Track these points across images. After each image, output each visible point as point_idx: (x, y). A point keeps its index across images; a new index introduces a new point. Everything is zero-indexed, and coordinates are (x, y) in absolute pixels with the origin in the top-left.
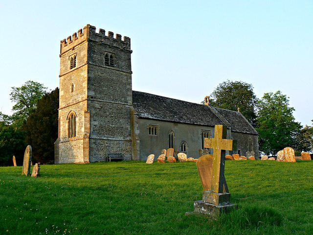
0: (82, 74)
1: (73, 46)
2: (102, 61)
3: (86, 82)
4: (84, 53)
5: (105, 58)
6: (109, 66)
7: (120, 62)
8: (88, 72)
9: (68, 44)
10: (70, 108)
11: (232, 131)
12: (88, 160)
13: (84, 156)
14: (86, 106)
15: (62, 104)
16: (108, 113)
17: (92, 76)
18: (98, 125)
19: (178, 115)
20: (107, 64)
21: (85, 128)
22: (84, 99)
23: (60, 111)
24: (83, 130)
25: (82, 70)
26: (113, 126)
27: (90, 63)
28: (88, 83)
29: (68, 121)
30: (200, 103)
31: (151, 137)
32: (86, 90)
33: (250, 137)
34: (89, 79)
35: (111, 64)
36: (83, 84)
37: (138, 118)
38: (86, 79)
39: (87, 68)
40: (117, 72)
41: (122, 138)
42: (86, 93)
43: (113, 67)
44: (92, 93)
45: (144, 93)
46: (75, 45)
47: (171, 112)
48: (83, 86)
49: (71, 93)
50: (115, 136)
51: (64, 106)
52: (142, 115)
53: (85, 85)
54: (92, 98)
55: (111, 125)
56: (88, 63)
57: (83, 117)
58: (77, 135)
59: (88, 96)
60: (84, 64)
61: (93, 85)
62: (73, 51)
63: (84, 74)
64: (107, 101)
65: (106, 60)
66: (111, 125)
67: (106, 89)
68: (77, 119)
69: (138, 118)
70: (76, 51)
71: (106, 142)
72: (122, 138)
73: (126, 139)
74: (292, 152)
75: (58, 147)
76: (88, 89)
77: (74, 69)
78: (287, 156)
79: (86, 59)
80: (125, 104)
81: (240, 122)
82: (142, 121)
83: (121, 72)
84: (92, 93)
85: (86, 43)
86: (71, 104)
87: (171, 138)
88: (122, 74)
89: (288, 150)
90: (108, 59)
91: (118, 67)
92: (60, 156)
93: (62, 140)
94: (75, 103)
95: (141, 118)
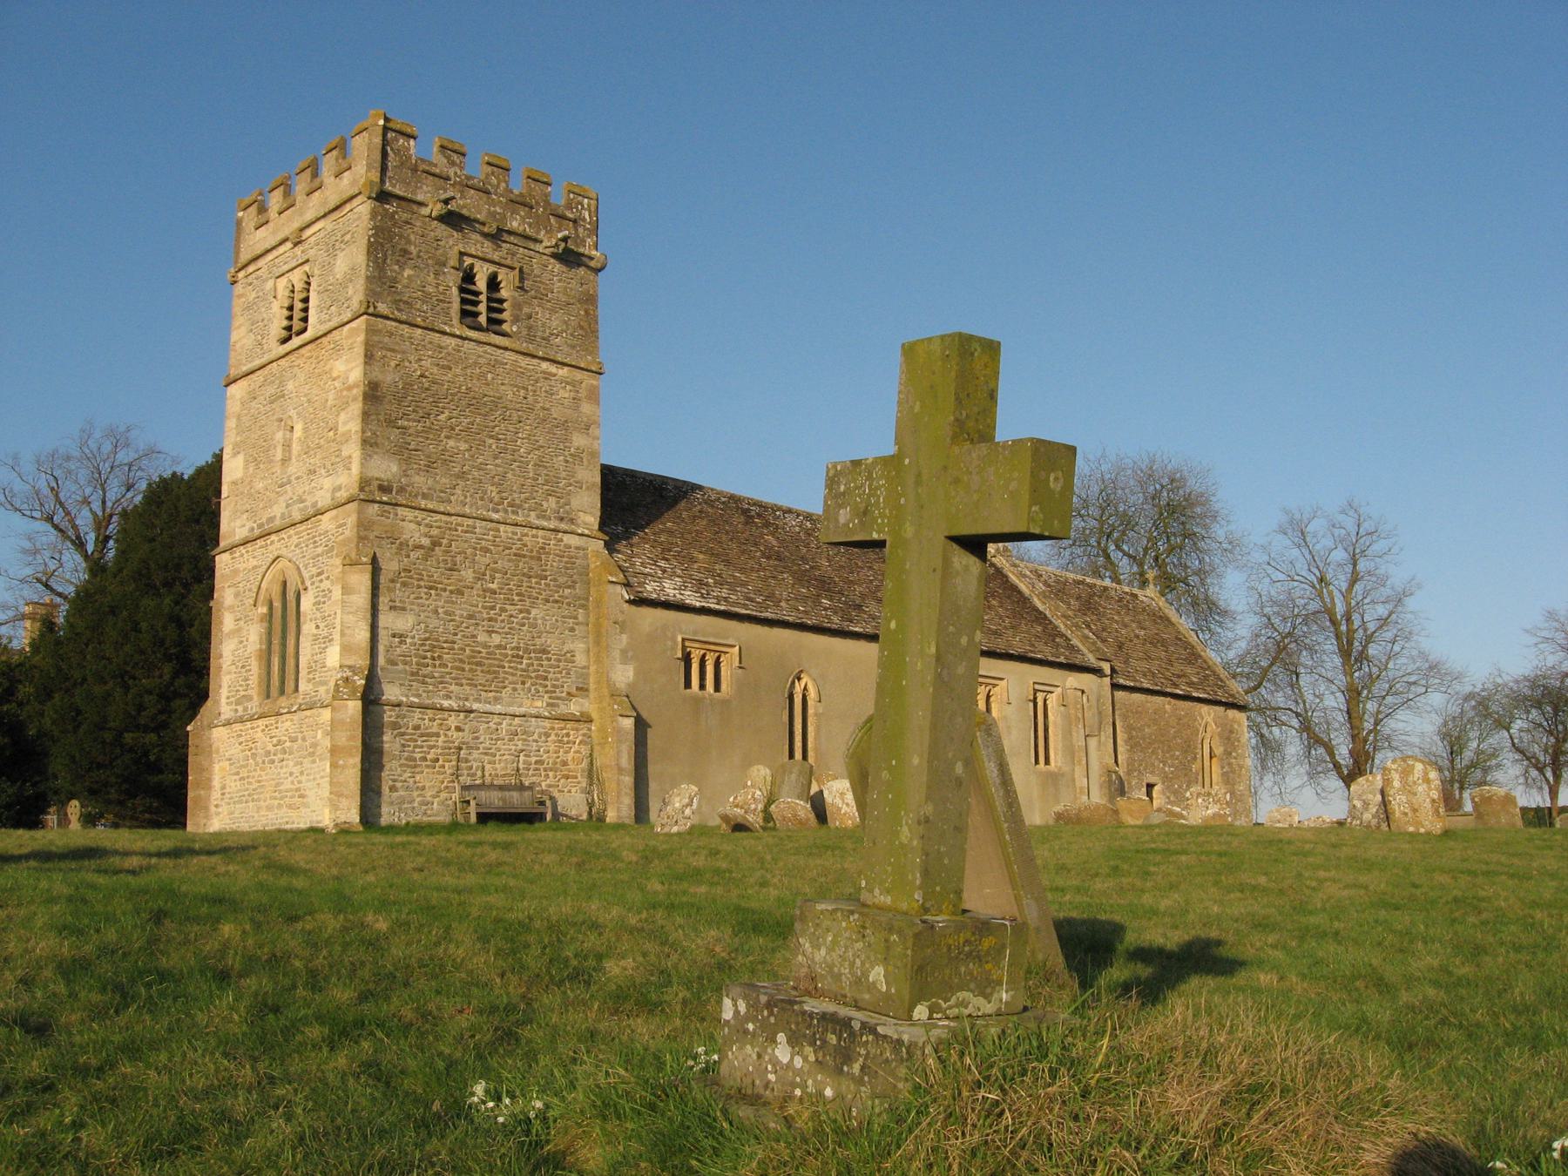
0: (339, 366)
1: (297, 225)
2: (444, 301)
3: (356, 408)
4: (351, 261)
5: (462, 290)
6: (478, 328)
7: (541, 315)
8: (369, 357)
9: (273, 213)
10: (275, 545)
11: (1115, 686)
12: (354, 816)
13: (337, 793)
14: (349, 531)
15: (233, 523)
16: (468, 575)
17: (388, 378)
18: (419, 635)
19: (841, 593)
20: (468, 315)
21: (346, 649)
22: (343, 495)
23: (223, 562)
24: (333, 656)
25: (338, 349)
26: (496, 639)
27: (382, 308)
28: (366, 415)
29: (263, 610)
30: (807, 497)
31: (697, 701)
32: (353, 450)
33: (1208, 714)
34: (373, 394)
35: (490, 320)
36: (343, 417)
37: (630, 602)
38: (358, 392)
39: (361, 338)
40: (524, 362)
41: (540, 705)
42: (355, 468)
43: (504, 334)
44: (386, 468)
45: (665, 480)
46: (309, 216)
47: (801, 577)
48: (341, 429)
49: (277, 469)
50: (505, 694)
51: (241, 533)
52: (650, 589)
53: (350, 422)
54: (386, 489)
55: (482, 637)
56: (369, 311)
57: (337, 593)
58: (302, 687)
59: (364, 483)
60: (349, 315)
61: (391, 423)
62: (298, 250)
63: (349, 368)
64: (467, 510)
65: (463, 301)
66: (482, 637)
67: (463, 446)
68: (307, 603)
69: (630, 602)
70: (310, 249)
71: (453, 721)
72: (540, 705)
73: (563, 709)
74: (1427, 781)
75: (208, 751)
76: (365, 442)
77: (296, 341)
78: (1398, 803)
79: (356, 294)
80: (563, 526)
81: (1157, 641)
82: (650, 618)
83: (545, 365)
84: (386, 468)
85: (363, 209)
86: (278, 523)
87: (793, 709)
88: (548, 376)
89: (758, 770)
90: (477, 294)
91: (531, 338)
92: (215, 795)
93: (226, 711)
94: (297, 516)
95: (640, 601)
